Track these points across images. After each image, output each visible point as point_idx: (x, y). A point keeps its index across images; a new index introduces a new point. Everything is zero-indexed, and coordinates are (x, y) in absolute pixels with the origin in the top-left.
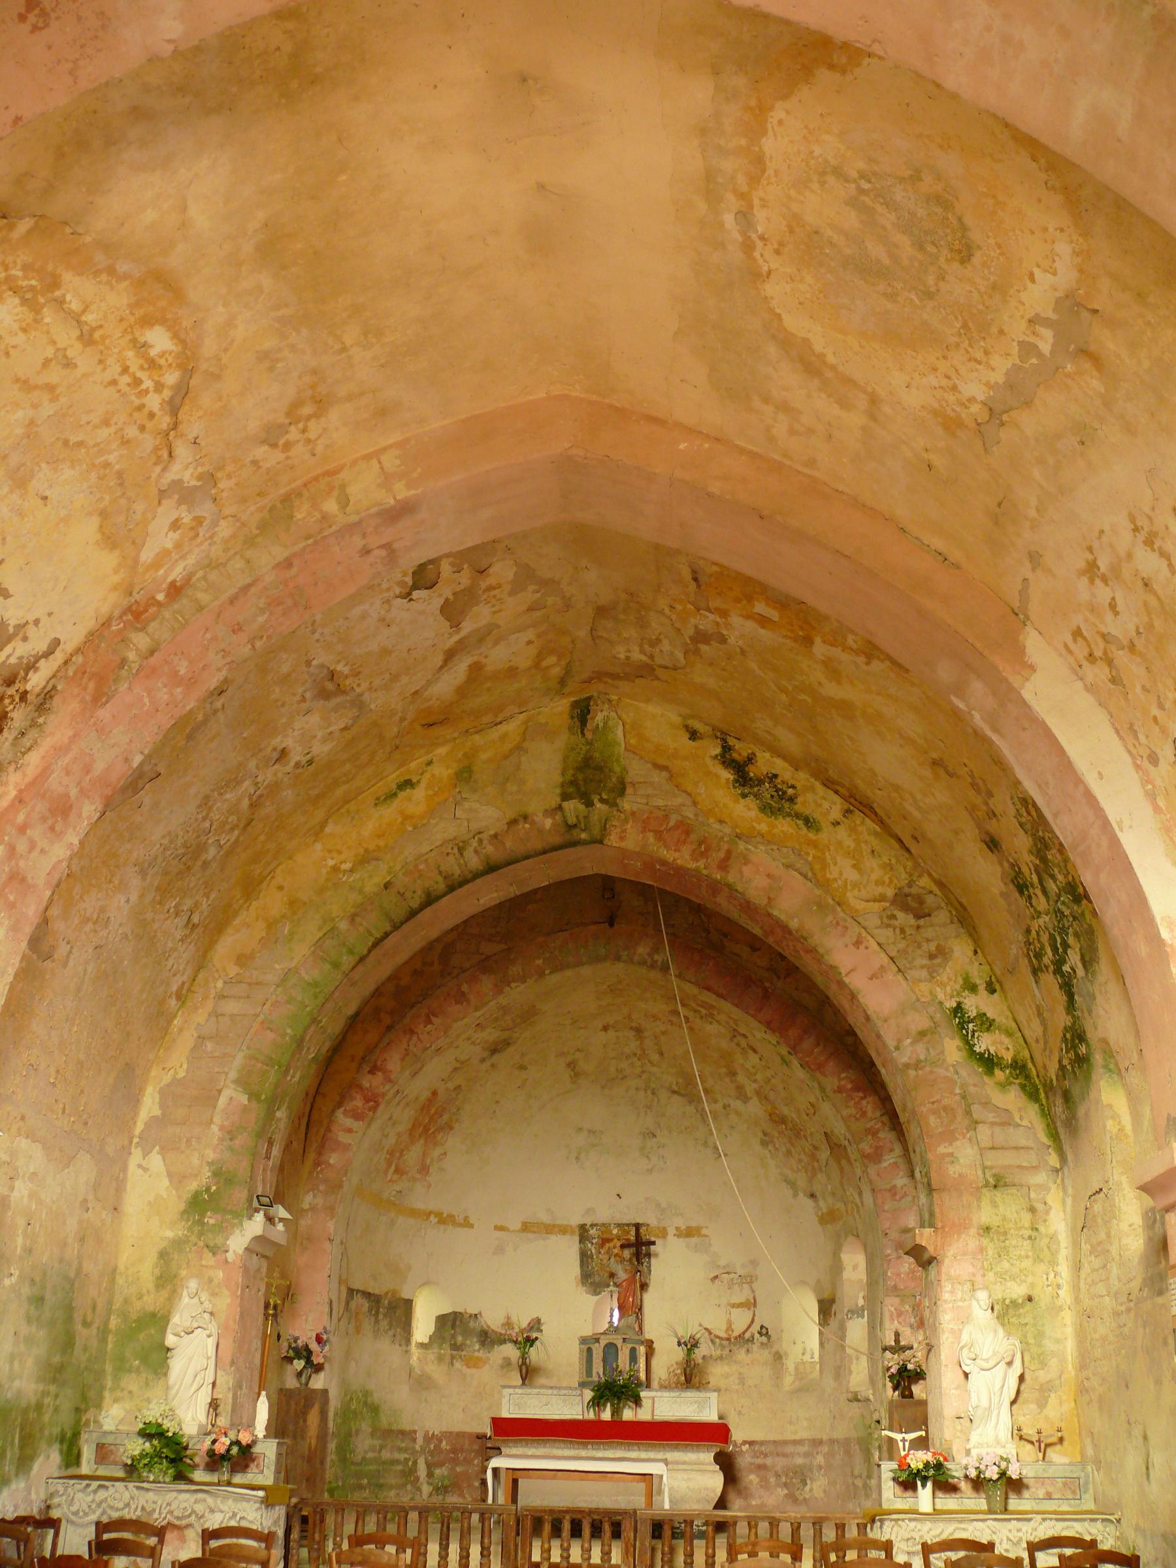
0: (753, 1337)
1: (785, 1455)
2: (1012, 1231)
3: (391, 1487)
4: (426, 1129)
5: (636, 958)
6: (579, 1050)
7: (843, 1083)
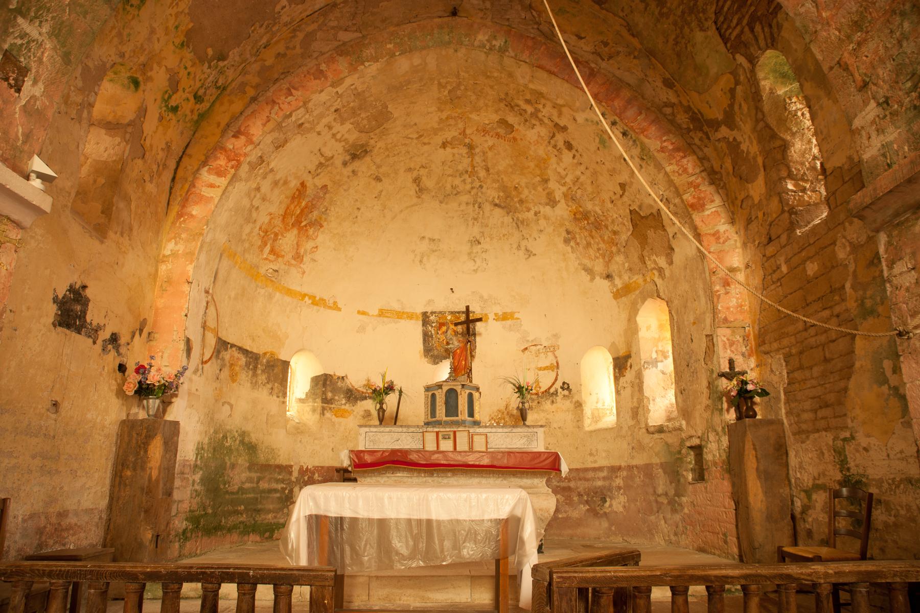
0: (556, 391)
1: (587, 480)
3: (269, 511)
4: (298, 222)
5: (476, 43)
6: (423, 167)
7: (665, 144)
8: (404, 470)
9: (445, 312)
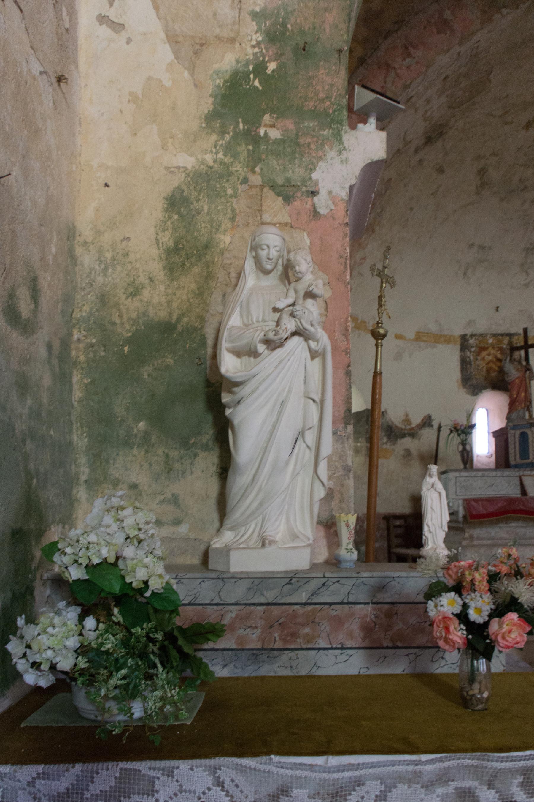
6: (493, 154)
8: (517, 519)
9: (487, 335)
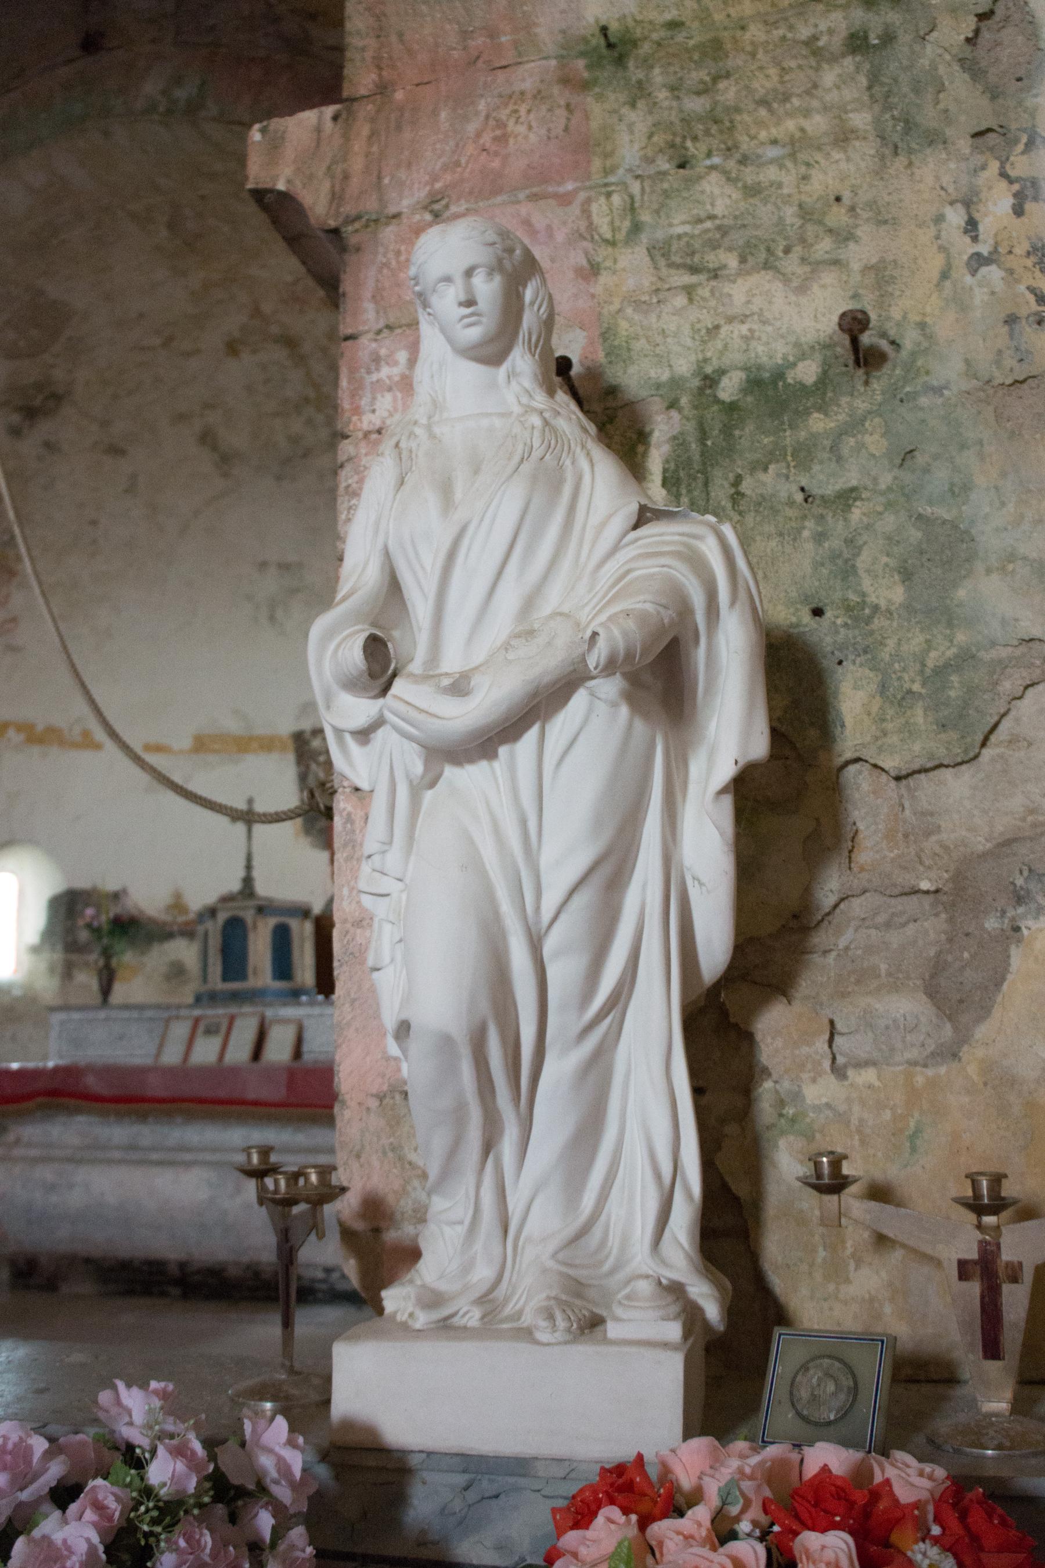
2: (756, 32)
